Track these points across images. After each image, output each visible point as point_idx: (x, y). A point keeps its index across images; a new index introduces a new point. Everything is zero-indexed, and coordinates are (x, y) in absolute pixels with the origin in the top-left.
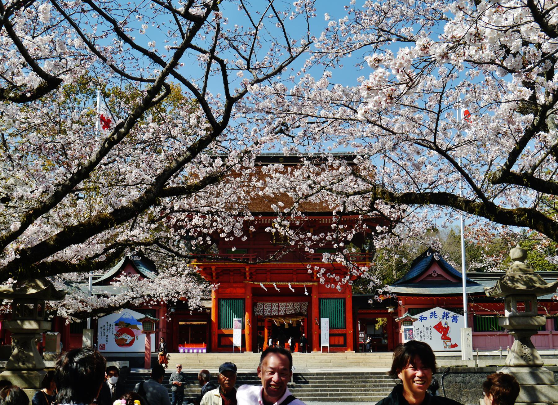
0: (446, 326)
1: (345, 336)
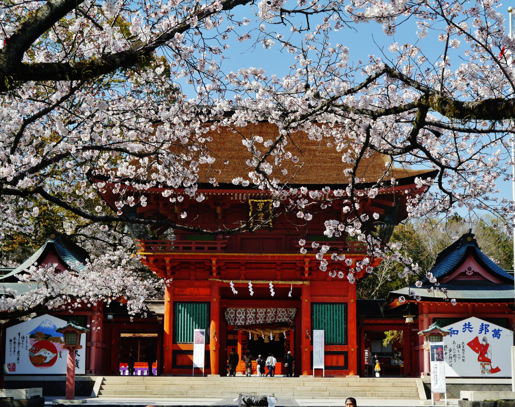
0: (484, 343)
1: (346, 354)
